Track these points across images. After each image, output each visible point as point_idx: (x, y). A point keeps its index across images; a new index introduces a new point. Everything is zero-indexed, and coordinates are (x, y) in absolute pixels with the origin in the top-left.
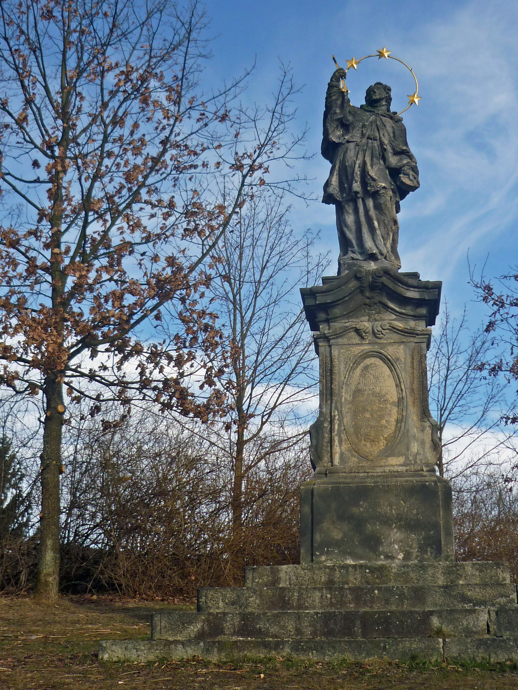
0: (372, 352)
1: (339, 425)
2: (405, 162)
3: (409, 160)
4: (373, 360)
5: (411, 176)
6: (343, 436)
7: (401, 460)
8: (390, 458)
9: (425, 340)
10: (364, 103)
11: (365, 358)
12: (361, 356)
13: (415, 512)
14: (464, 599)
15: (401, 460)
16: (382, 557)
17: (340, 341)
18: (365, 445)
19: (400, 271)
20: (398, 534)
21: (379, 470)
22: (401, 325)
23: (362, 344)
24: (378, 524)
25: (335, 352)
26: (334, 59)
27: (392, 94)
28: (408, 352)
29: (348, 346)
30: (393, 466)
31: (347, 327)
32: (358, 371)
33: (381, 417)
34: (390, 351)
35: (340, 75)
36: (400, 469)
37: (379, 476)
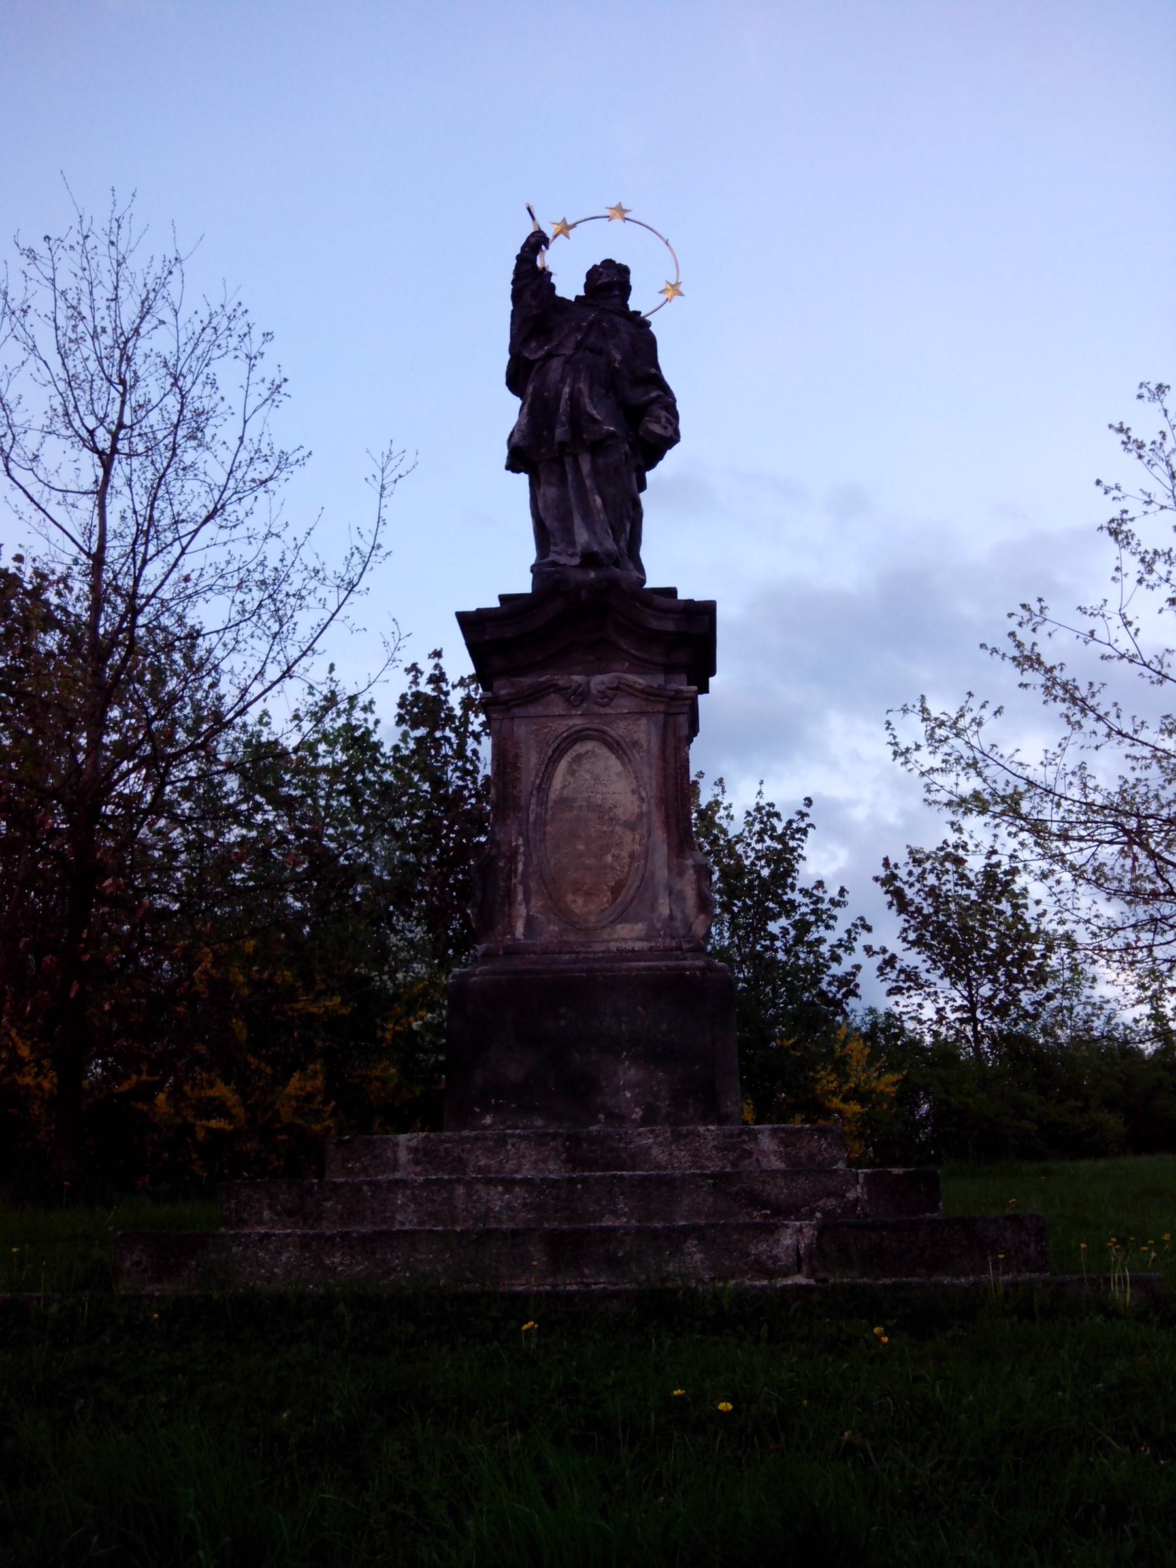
0: (588, 729)
1: (526, 865)
2: (653, 395)
3: (660, 393)
4: (589, 745)
5: (663, 420)
6: (533, 885)
7: (640, 928)
8: (619, 926)
9: (686, 709)
10: (583, 294)
11: (575, 742)
12: (567, 737)
13: (664, 1027)
14: (754, 1200)
15: (640, 928)
16: (602, 1116)
17: (532, 710)
18: (574, 901)
19: (646, 586)
20: (632, 1072)
21: (598, 947)
22: (641, 681)
23: (570, 716)
24: (593, 1050)
25: (521, 730)
26: (529, 209)
27: (633, 281)
28: (653, 730)
29: (543, 720)
30: (624, 940)
31: (541, 683)
32: (563, 765)
33: (606, 849)
34: (619, 730)
35: (537, 242)
36: (638, 945)
37: (598, 960)
